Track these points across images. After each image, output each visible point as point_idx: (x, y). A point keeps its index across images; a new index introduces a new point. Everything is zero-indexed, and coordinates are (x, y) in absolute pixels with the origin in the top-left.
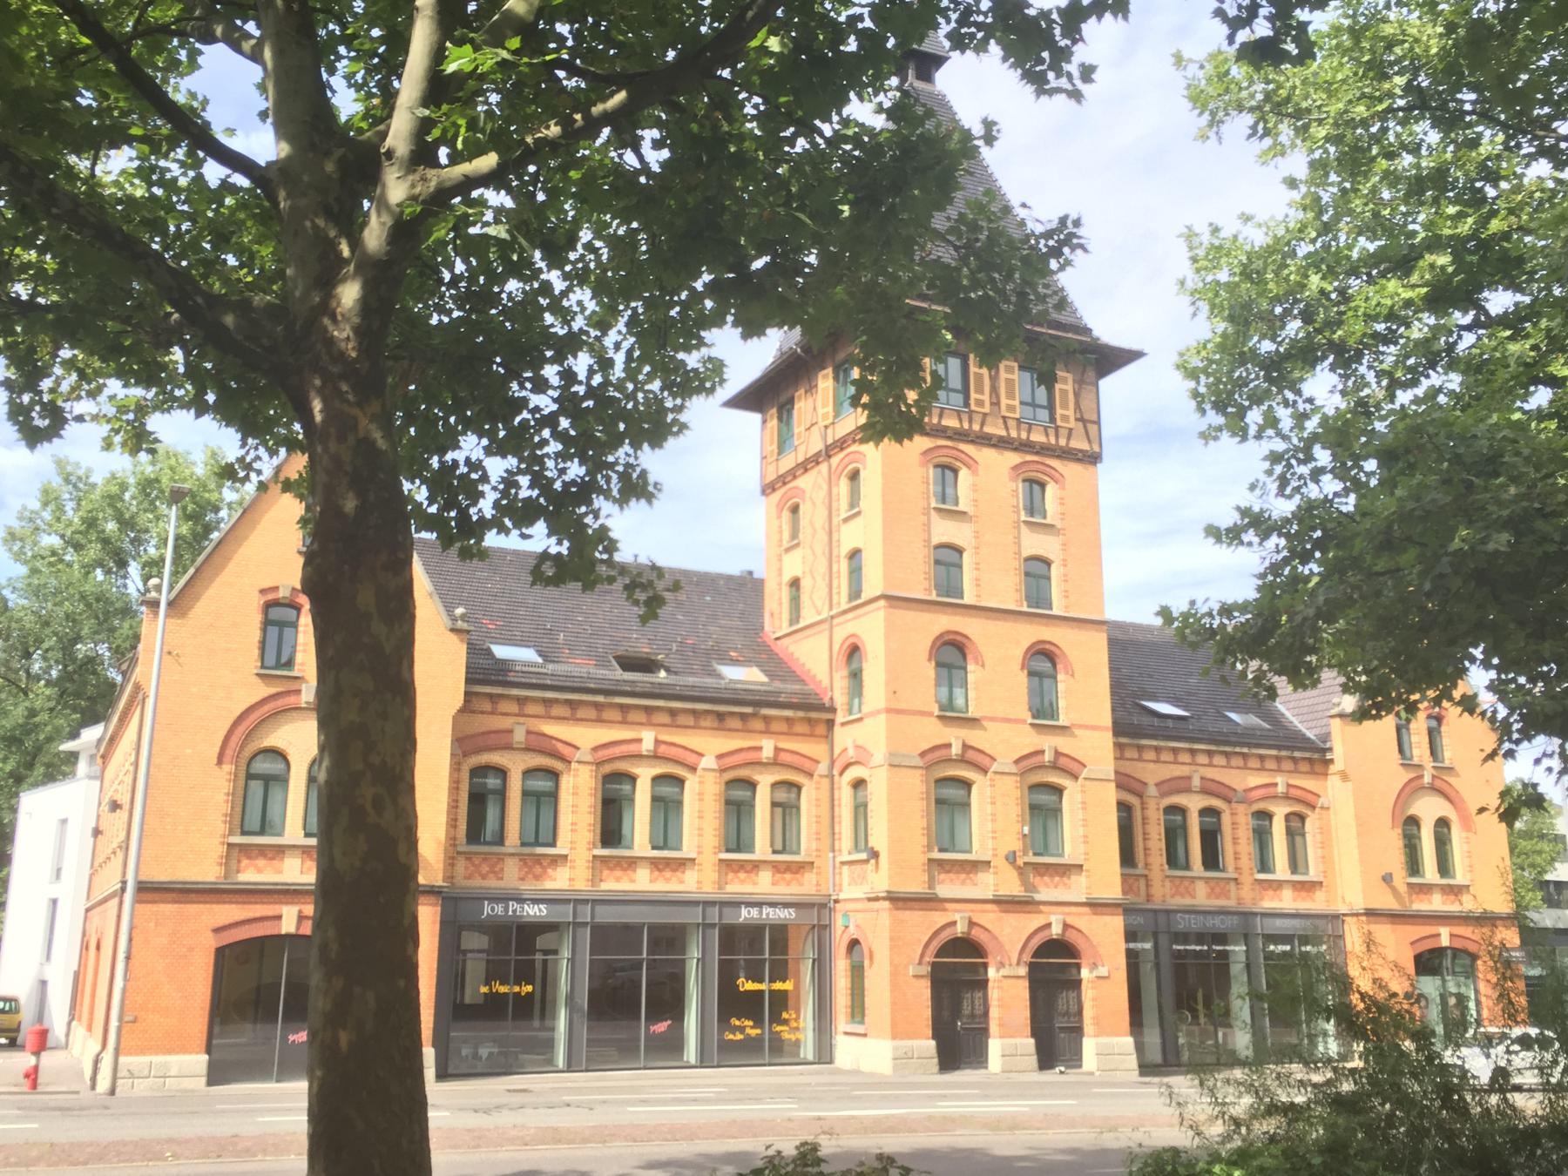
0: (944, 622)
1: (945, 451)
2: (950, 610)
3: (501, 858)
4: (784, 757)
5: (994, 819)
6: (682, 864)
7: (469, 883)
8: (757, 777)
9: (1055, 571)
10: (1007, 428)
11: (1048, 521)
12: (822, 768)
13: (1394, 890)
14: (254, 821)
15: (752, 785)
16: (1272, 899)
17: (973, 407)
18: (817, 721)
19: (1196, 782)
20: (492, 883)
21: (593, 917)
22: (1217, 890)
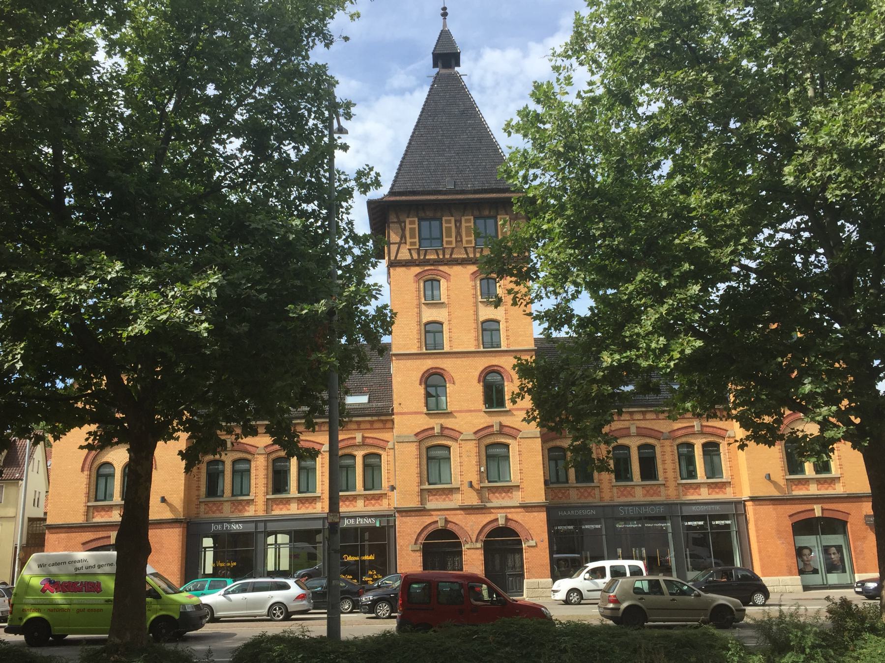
0: (429, 363)
1: (427, 273)
2: (433, 356)
3: (222, 503)
4: (368, 441)
5: (464, 464)
6: (834, 480)
7: (207, 516)
8: (355, 453)
9: (445, 328)
10: (467, 254)
11: (442, 301)
12: (390, 445)
13: (775, 484)
14: (101, 495)
15: (691, 446)
16: (693, 494)
17: (445, 246)
18: (387, 421)
19: (633, 430)
20: (218, 515)
21: (265, 528)
22: (652, 492)
